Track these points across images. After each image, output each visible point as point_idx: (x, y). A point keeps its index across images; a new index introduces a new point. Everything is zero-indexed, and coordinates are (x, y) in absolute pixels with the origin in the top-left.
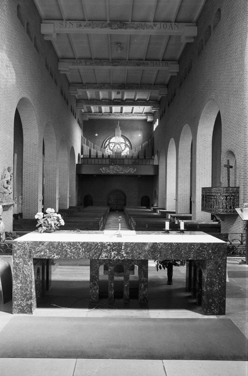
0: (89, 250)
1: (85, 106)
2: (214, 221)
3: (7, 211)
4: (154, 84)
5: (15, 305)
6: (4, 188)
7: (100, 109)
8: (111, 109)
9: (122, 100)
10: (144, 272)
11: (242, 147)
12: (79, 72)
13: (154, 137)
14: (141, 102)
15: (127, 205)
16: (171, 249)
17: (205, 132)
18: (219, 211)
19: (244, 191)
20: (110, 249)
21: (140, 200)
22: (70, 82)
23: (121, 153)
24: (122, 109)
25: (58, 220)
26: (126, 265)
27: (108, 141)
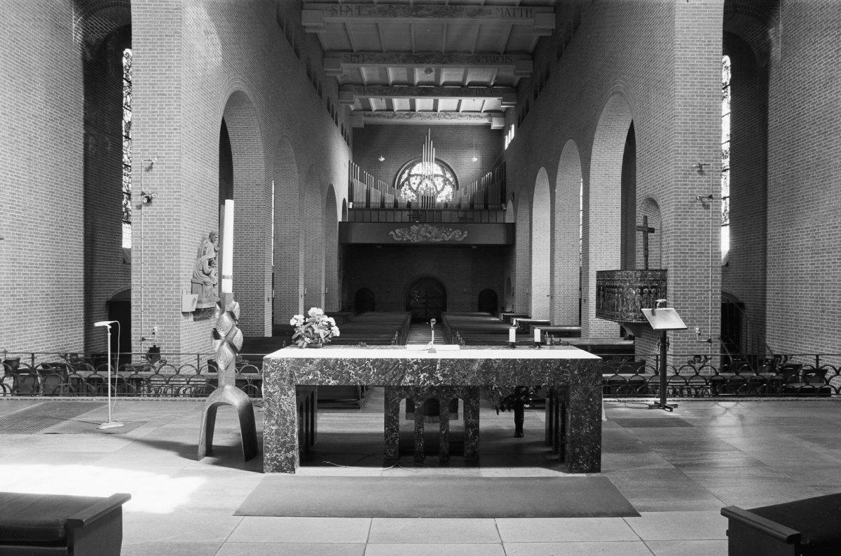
0: (384, 372)
1: (357, 99)
2: (625, 339)
3: (208, 320)
4: (505, 53)
5: (268, 459)
6: (204, 273)
7: (390, 103)
8: (413, 104)
9: (436, 84)
10: (473, 411)
11: (671, 193)
12: (345, 29)
13: (505, 163)
14: (477, 89)
15: (448, 310)
16: (514, 368)
17: (607, 158)
18: (628, 317)
19: (675, 277)
20: (418, 369)
21: (476, 300)
22: (325, 50)
23: (433, 198)
24: (436, 103)
25: (329, 326)
26: (445, 399)
27: (407, 171)
